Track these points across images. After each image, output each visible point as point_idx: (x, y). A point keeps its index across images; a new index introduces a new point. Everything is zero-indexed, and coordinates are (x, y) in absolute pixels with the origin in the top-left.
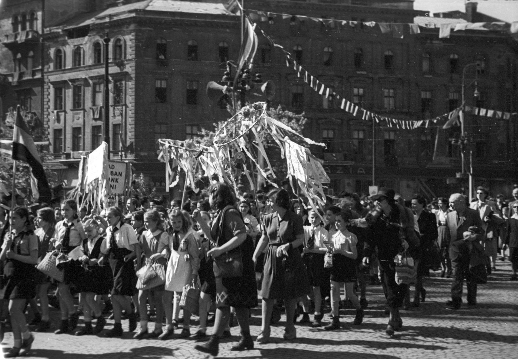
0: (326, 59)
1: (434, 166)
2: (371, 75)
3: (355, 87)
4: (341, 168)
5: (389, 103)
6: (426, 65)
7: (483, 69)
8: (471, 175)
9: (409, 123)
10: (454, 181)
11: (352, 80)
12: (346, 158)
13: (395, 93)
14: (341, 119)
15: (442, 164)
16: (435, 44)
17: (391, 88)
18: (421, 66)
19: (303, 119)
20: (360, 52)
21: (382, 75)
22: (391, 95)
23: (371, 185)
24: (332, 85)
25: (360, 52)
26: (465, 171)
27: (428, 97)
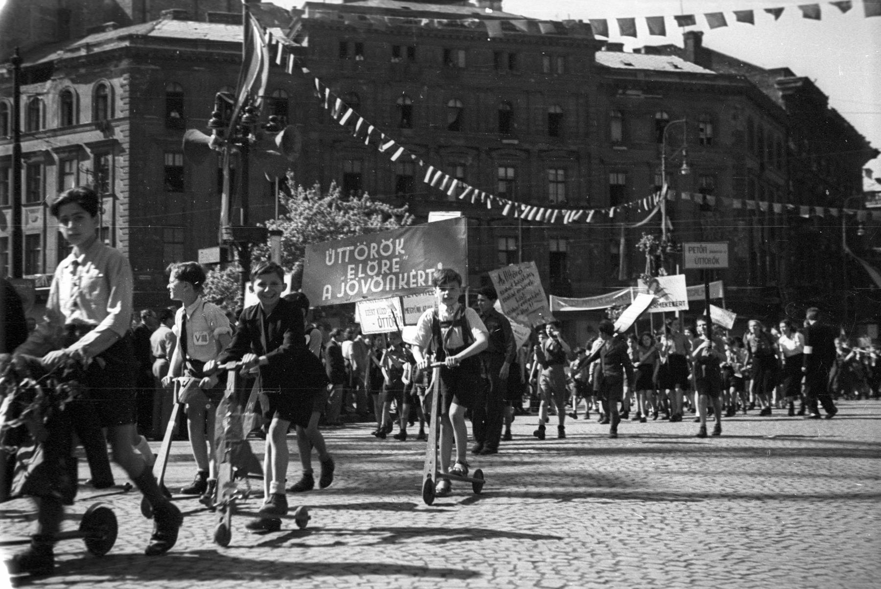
0: (451, 119)
2: (526, 146)
3: (501, 166)
5: (557, 192)
6: (616, 132)
11: (494, 154)
13: (566, 176)
14: (477, 219)
18: (608, 133)
19: (408, 217)
20: (508, 108)
21: (542, 146)
22: (560, 178)
25: (508, 108)
27: (620, 182)
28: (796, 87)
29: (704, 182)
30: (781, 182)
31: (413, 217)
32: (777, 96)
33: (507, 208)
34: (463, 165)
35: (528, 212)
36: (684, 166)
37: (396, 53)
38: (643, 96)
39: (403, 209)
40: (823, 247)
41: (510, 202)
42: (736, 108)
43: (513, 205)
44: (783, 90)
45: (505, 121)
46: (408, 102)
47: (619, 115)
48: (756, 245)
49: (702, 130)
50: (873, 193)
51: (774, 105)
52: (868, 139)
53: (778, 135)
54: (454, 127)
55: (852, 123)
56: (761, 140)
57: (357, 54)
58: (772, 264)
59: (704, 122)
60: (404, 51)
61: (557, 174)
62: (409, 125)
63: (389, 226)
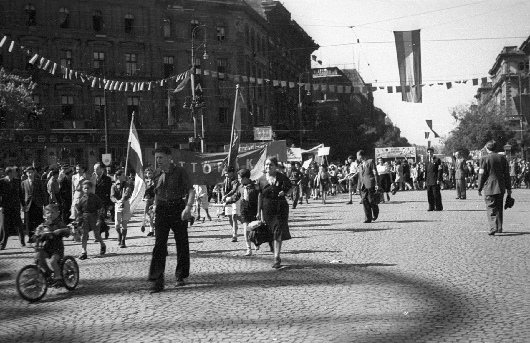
0: (62, 20)
1: (178, 132)
2: (111, 39)
3: (95, 51)
4: (83, 136)
5: (131, 69)
6: (167, 31)
8: (203, 139)
9: (69, 72)
10: (187, 146)
11: (91, 44)
12: (86, 126)
13: (137, 58)
17: (134, 53)
18: (162, 31)
19: (32, 84)
20: (99, 14)
21: (122, 39)
22: (133, 60)
23: (104, 153)
25: (99, 14)
26: (197, 136)
27: (170, 63)
28: (272, 7)
29: (220, 63)
30: (265, 63)
31: (35, 84)
32: (262, 12)
33: (94, 81)
34: (71, 51)
35: (108, 85)
36: (205, 54)
39: (28, 79)
40: (289, 101)
41: (95, 78)
42: (238, 19)
43: (97, 80)
44: (266, 8)
45: (97, 23)
46: (33, 8)
47: (169, 21)
48: (251, 101)
49: (219, 31)
50: (317, 70)
51: (260, 17)
52: (313, 39)
53: (263, 35)
54: (65, 26)
55: (304, 29)
56: (253, 38)
58: (261, 112)
61: (131, 57)
62: (34, 24)
63: (19, 90)
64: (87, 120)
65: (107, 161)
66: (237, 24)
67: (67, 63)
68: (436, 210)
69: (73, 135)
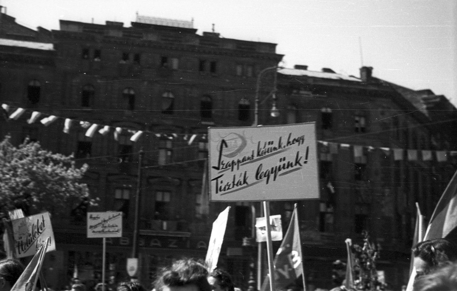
0: (165, 107)
4: (175, 241)
7: (363, 126)
14: (179, 179)
15: (311, 240)
16: (303, 94)
20: (209, 100)
24: (427, 247)
32: (423, 108)
36: (274, 109)
37: (125, 57)
38: (312, 95)
42: (383, 107)
46: (132, 92)
49: (357, 122)
54: (169, 111)
57: (96, 57)
59: (360, 116)
60: (131, 57)
64: (182, 221)
65: (132, 269)
66: (383, 113)
67: (167, 153)
68: (236, 77)
69: (162, 239)
